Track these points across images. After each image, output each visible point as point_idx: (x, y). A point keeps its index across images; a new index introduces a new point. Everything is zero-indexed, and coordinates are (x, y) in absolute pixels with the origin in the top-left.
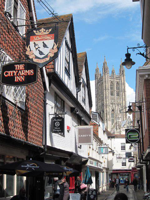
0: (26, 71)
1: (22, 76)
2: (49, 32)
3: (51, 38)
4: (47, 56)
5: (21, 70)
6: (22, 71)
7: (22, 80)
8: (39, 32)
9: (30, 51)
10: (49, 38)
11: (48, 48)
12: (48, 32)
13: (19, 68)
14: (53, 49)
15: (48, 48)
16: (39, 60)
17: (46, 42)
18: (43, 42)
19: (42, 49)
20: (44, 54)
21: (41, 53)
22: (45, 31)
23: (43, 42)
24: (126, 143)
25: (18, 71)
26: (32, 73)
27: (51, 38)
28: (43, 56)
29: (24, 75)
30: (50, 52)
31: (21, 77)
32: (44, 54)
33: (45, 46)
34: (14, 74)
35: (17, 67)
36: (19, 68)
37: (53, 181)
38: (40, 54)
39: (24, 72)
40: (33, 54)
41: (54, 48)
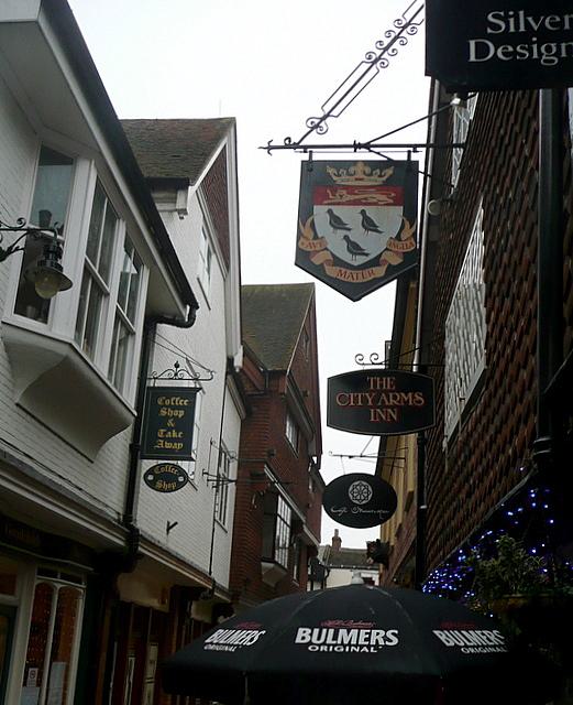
0: (403, 394)
1: (392, 407)
2: (384, 179)
3: (391, 201)
4: (376, 262)
5: (387, 392)
6: (391, 395)
7: (391, 417)
8: (348, 174)
9: (316, 237)
10: (384, 198)
11: (380, 232)
12: (381, 176)
13: (381, 385)
14: (398, 237)
15: (380, 232)
16: (349, 271)
17: (371, 212)
18: (363, 212)
19: (358, 234)
20: (367, 255)
21: (355, 248)
22: (371, 175)
23: (363, 212)
24: (308, 168)
25: (379, 393)
26: (420, 402)
27: (391, 201)
28: (361, 260)
29: (395, 406)
30: (387, 249)
31: (389, 410)
32: (367, 255)
33: (369, 224)
34: (365, 400)
35: (375, 382)
36: (381, 385)
37: (380, 590)
38: (335, 228)
39: (395, 397)
40: (326, 249)
41: (403, 237)
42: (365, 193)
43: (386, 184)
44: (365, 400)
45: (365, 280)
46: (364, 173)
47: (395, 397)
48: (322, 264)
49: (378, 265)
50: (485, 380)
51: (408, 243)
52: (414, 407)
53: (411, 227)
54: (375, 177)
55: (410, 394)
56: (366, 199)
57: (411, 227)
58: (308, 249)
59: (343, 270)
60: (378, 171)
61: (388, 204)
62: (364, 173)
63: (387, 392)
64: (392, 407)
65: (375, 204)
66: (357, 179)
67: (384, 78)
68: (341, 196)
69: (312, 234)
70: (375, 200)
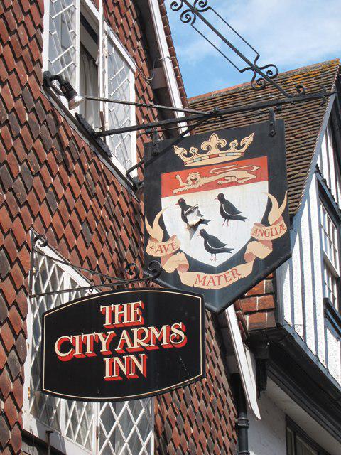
0: (153, 329)
1: (136, 354)
2: (243, 150)
4: (240, 258)
6: (135, 331)
7: (122, 360)
8: (201, 152)
9: (166, 238)
10: (244, 174)
12: (239, 147)
14: (265, 222)
15: (242, 219)
16: (209, 276)
17: (231, 194)
19: (218, 226)
21: (214, 245)
22: (227, 147)
25: (118, 331)
26: (178, 339)
28: (222, 258)
29: (145, 350)
30: (252, 239)
31: (133, 357)
32: (228, 251)
33: (229, 212)
40: (180, 251)
41: (271, 219)
42: (224, 171)
43: (250, 154)
44: (97, 345)
45: (229, 283)
46: (219, 147)
47: (142, 335)
48: (176, 271)
49: (244, 262)
50: (251, 274)
51: (278, 226)
52: (172, 351)
53: (280, 205)
54: (232, 149)
55: (164, 327)
56: (223, 179)
57: (280, 205)
58: (159, 255)
59: (202, 275)
60: (236, 141)
61: (252, 181)
62: (219, 147)
63: (129, 329)
64: (136, 354)
65: (235, 183)
66: (211, 157)
67: (205, 17)
68: (194, 181)
69: (161, 232)
70: (234, 179)
